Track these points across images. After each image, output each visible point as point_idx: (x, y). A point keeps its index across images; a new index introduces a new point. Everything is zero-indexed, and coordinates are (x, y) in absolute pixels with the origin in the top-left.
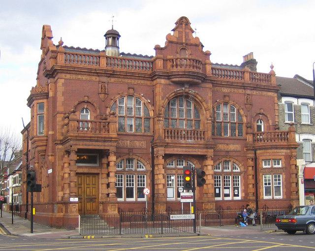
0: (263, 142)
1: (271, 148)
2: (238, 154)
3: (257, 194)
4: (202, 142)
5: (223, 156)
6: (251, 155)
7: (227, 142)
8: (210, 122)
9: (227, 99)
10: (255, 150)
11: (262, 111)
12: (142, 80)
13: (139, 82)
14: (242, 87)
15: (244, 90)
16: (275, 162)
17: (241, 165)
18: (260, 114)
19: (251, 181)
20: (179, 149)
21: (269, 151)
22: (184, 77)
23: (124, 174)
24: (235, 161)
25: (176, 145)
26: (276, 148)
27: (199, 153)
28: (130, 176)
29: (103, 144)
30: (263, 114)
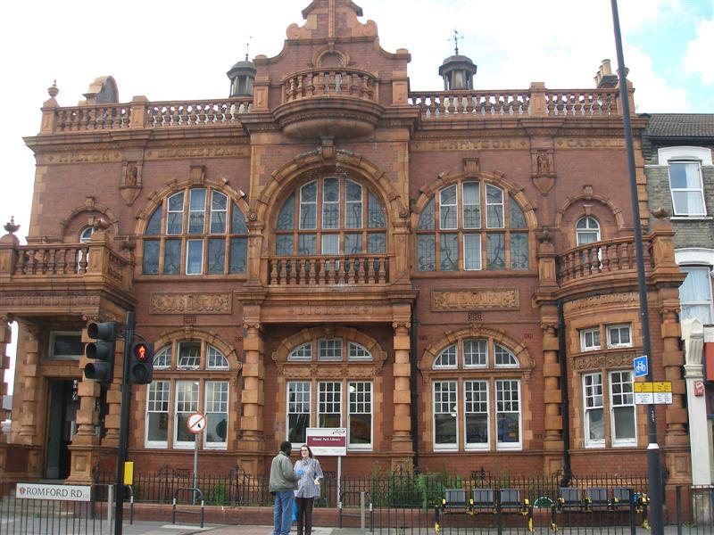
0: (578, 275)
1: (598, 293)
2: (513, 317)
3: (565, 433)
4: (382, 285)
5: (462, 326)
6: (549, 319)
7: (471, 284)
8: (403, 230)
9: (472, 167)
10: (559, 304)
11: (589, 191)
12: (227, 144)
13: (221, 151)
14: (522, 133)
15: (527, 142)
16: (614, 332)
17: (518, 349)
18: (584, 200)
19: (552, 394)
20: (307, 310)
21: (594, 300)
22: (308, 119)
23: (457, 379)
24: (499, 338)
25: (292, 301)
26: (613, 291)
27: (369, 319)
28: (330, 385)
29: (67, 300)
30: (593, 200)
